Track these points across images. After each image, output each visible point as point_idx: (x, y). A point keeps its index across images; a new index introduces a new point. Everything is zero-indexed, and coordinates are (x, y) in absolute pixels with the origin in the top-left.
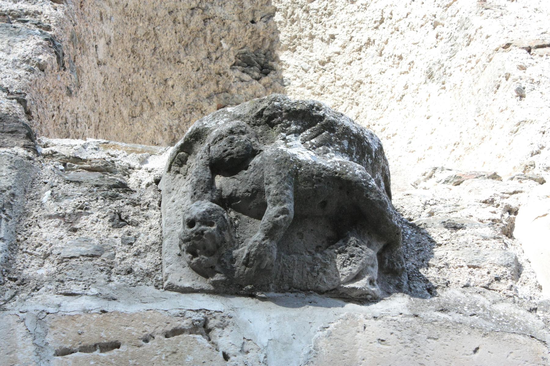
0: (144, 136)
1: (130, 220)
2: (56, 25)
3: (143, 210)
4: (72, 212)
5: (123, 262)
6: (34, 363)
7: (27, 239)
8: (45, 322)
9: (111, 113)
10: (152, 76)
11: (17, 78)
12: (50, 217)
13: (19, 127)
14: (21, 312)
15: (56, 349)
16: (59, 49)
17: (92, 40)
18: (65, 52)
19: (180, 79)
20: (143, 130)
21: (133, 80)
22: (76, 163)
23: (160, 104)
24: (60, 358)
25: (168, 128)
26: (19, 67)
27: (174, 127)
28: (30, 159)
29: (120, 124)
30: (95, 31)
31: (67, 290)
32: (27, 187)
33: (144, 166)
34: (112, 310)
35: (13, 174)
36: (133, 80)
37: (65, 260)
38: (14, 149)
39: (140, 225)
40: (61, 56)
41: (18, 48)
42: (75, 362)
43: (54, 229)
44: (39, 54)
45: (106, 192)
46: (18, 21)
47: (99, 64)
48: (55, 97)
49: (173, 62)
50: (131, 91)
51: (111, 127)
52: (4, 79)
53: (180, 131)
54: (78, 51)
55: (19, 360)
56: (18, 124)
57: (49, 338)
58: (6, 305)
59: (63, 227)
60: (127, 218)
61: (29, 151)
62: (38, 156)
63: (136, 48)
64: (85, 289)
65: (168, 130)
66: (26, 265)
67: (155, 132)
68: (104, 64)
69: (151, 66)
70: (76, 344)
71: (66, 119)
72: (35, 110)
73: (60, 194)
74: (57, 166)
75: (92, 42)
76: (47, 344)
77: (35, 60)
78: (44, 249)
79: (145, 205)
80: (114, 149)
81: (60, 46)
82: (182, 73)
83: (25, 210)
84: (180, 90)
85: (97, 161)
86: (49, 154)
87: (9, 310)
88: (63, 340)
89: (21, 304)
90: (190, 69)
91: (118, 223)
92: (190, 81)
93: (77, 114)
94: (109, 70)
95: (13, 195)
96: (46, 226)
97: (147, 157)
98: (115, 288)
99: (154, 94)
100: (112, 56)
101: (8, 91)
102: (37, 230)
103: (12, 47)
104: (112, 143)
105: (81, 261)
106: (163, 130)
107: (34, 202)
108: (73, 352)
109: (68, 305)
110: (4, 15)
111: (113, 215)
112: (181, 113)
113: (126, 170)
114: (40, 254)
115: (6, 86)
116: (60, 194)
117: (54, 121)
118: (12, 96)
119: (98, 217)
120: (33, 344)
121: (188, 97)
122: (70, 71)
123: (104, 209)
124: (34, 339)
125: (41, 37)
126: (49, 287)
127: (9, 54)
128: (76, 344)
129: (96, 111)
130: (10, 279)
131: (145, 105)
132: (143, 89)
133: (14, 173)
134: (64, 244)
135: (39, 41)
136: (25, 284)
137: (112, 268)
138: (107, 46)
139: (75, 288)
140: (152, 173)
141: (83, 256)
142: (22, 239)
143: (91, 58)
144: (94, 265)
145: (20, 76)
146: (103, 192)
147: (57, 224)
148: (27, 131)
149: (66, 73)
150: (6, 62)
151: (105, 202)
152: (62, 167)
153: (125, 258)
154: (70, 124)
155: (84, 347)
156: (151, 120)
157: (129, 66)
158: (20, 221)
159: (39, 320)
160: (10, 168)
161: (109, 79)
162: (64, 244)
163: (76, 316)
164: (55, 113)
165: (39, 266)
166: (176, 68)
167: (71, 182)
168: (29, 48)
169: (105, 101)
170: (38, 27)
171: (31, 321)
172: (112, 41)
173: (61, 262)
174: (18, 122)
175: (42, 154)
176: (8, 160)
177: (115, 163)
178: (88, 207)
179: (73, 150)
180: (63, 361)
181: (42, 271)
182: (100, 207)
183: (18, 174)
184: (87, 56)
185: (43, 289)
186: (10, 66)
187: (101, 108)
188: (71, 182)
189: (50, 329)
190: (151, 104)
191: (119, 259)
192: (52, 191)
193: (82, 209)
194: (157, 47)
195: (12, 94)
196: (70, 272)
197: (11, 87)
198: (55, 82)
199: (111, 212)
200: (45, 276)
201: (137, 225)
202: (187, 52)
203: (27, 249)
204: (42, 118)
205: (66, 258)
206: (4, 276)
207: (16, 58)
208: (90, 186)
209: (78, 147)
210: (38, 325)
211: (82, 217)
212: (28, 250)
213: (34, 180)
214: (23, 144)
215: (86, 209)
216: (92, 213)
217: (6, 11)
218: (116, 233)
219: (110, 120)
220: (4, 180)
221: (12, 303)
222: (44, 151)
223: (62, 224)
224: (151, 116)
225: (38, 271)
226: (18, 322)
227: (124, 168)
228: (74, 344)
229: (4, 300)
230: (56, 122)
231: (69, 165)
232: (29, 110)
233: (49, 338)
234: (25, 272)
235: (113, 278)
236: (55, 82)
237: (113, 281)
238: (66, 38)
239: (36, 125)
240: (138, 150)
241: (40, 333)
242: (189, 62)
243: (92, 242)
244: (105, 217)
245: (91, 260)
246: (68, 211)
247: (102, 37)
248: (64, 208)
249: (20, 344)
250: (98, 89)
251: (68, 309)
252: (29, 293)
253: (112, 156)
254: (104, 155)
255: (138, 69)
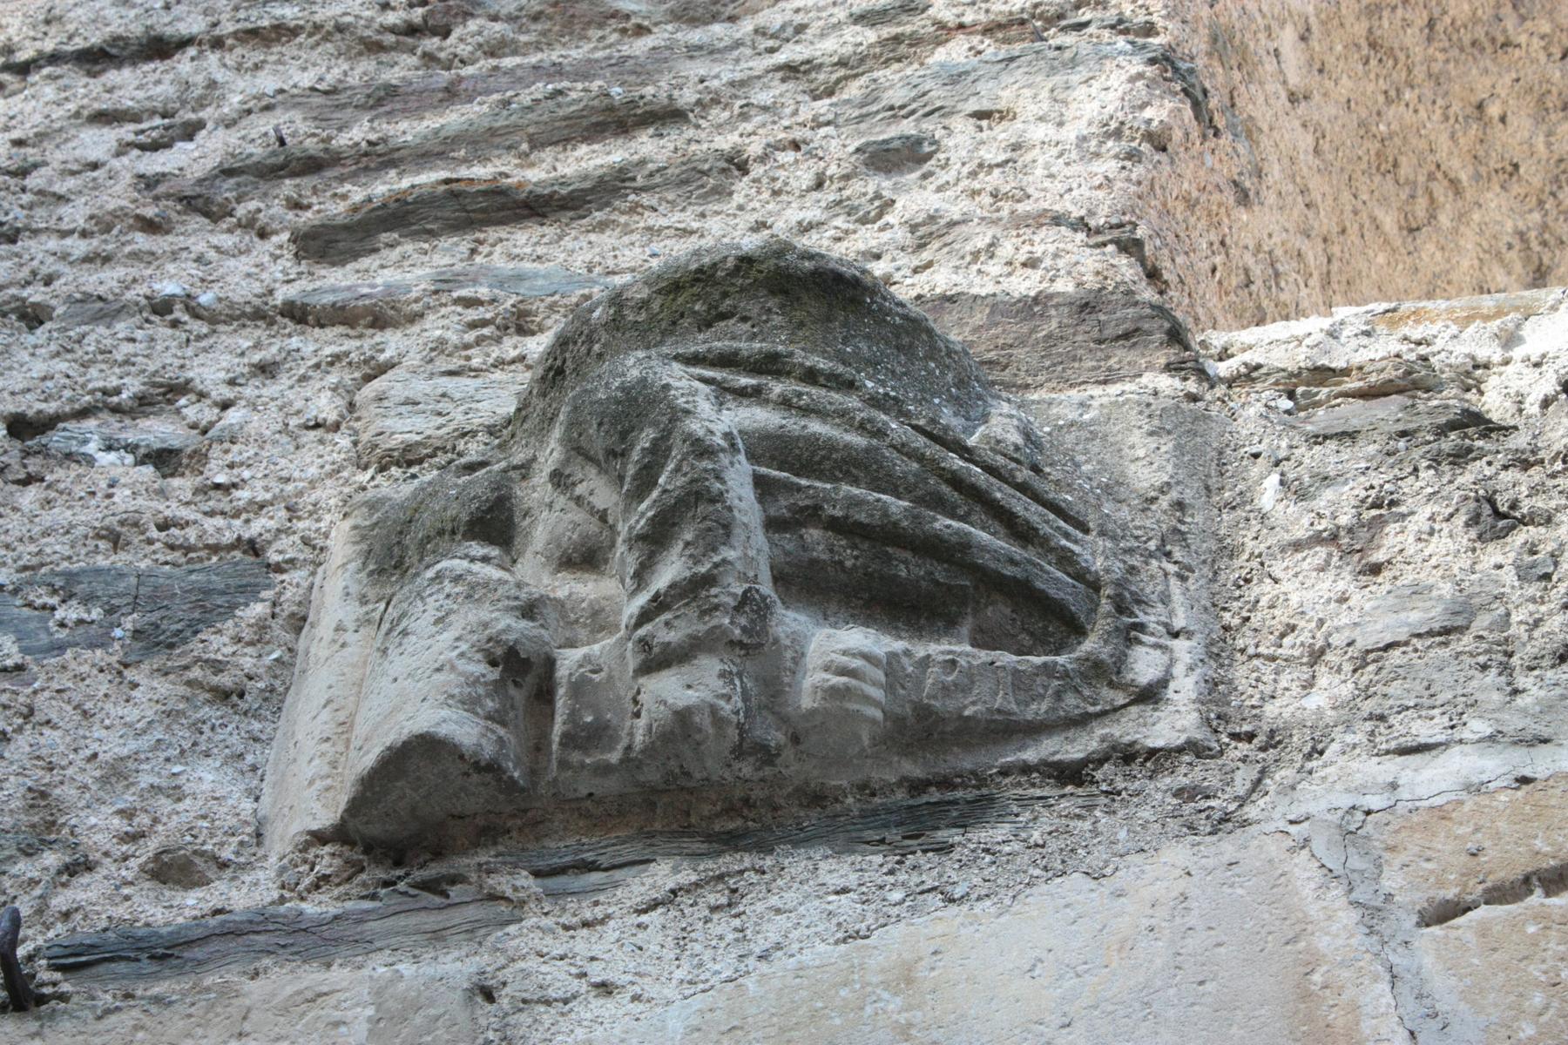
0: (1454, 276)
1: (1525, 511)
2: (1168, 17)
3: (1553, 476)
4: (1355, 521)
5: (1536, 634)
6: (1368, 956)
7: (1248, 619)
8: (1367, 838)
9: (1353, 230)
10: (1440, 102)
11: (1100, 187)
12: (1297, 546)
13: (1142, 318)
14: (1292, 822)
15: (1418, 907)
16: (1193, 80)
17: (1262, 36)
18: (1207, 85)
19: (1518, 94)
20: (1448, 261)
21: (1389, 125)
22: (1321, 384)
23: (1477, 177)
24: (1436, 930)
25: (1516, 242)
26: (1097, 155)
27: (1533, 234)
28: (1194, 398)
29: (1381, 259)
30: (1265, 8)
31: (1402, 740)
32: (1208, 476)
33: (1517, 353)
34: (1548, 773)
35: (1164, 449)
36: (1389, 125)
37: (1371, 656)
38: (1144, 380)
39: (1556, 520)
40: (1200, 97)
41: (1081, 102)
42: (1484, 936)
43: (1318, 578)
44: (1143, 106)
45: (1435, 445)
46: (1063, 29)
47: (1293, 98)
48: (1209, 215)
49: (1489, 50)
50: (1391, 159)
51: (1360, 272)
52: (1066, 196)
53: (1552, 242)
54: (1237, 75)
55: (1324, 956)
56: (1137, 309)
57: (1392, 881)
58: (1246, 809)
59: (1340, 567)
60: (1514, 505)
61: (1185, 379)
62: (1212, 387)
63: (1379, 33)
64: (1452, 727)
65: (1518, 245)
66: (1268, 690)
67: (1481, 260)
68: (1305, 98)
69: (1430, 76)
70: (1471, 883)
71: (1246, 271)
72: (1168, 264)
73: (1306, 479)
74: (1273, 404)
75: (1263, 42)
76: (1389, 897)
77: (1136, 125)
78: (1305, 637)
79: (1554, 459)
80: (1417, 322)
81: (1191, 71)
82: (1522, 74)
83: (1220, 541)
84: (1527, 123)
85: (1379, 365)
86: (1239, 376)
87: (1258, 822)
88: (1432, 880)
89: (1287, 800)
90: (1542, 57)
91: (1493, 527)
92: (1549, 92)
93: (1270, 253)
94: (1323, 111)
95: (1180, 505)
96: (1291, 573)
97: (1518, 326)
98: (1538, 708)
99: (1456, 152)
100: (1321, 71)
101: (1086, 225)
102: (1269, 588)
103: (1065, 102)
104: (1407, 306)
105: (1416, 650)
106: (1504, 250)
107: (1240, 513)
108: (1469, 909)
109: (1419, 779)
110: (1023, 22)
111: (1472, 505)
112: (1543, 191)
113: (1468, 374)
114: (1296, 653)
115: (1076, 213)
116: (1306, 479)
117: (1220, 283)
118: (1100, 239)
119: (1432, 518)
120: (1351, 903)
121: (1552, 139)
122: (1231, 137)
123: (1444, 493)
124: (1351, 891)
125: (1136, 59)
126: (1349, 738)
127: (1061, 124)
128: (1471, 883)
129: (1313, 234)
130: (1235, 736)
131: (1439, 189)
132: (1422, 145)
133: (1167, 445)
134: (1356, 612)
135: (1134, 71)
136: (1280, 742)
137: (1510, 655)
138: (1303, 45)
139: (1423, 731)
140: (1544, 368)
141: (1419, 636)
142: (1236, 621)
143: (1271, 87)
144: (1458, 654)
145: (1106, 178)
146: (1427, 448)
147: (1321, 562)
148: (1167, 325)
149: (1222, 142)
150: (1060, 147)
151: (1439, 474)
152: (1289, 404)
153: (1541, 620)
154: (1259, 283)
155: (1495, 889)
156: (1462, 229)
157: (1371, 87)
158: (1215, 573)
159: (1348, 835)
160: (1151, 434)
161: (1328, 138)
162: (1356, 612)
163: (1450, 807)
164: (1218, 260)
165: (1304, 687)
166: (1500, 65)
167: (1326, 437)
168: (1111, 95)
169: (1329, 200)
170: (1121, 32)
171: (1329, 841)
172: (1315, 28)
173: (1361, 664)
174: (1136, 303)
175: (1221, 380)
176: (1141, 413)
177: (1432, 360)
178: (1395, 497)
179: (1304, 349)
180: (1446, 936)
181: (1317, 700)
182: (1430, 490)
183: (1178, 447)
184: (1261, 83)
185: (1335, 747)
186: (1074, 155)
187: (1325, 221)
188: (1326, 437)
189: (1387, 855)
190: (1454, 183)
191: (1523, 627)
192: (1282, 474)
193: (1380, 506)
194: (1436, 15)
195: (1098, 232)
196: (1395, 688)
197: (1091, 213)
198: (1202, 173)
199: (1466, 498)
200: (1329, 713)
201: (1549, 520)
202: (1523, 11)
203: (1257, 646)
204: (1189, 280)
205: (1372, 651)
206: (1216, 731)
207: (1085, 132)
208: (1385, 437)
209: (1318, 337)
210: (1351, 850)
211: (1387, 530)
212: (1261, 650)
213: (1221, 453)
214: (1163, 361)
215: (1392, 503)
216: (1412, 513)
217: (1023, 10)
218: (1493, 555)
219: (1353, 250)
220: (1146, 471)
221: (1261, 802)
222: (1223, 369)
223: (1335, 559)
224: (1461, 216)
225: (1305, 702)
226: (1292, 850)
227: (1461, 370)
228: (1465, 885)
229: (1236, 798)
230: (1225, 284)
231: (1303, 395)
232: (1154, 266)
233: (1392, 881)
234: (1270, 710)
235: (1522, 681)
236: (1202, 173)
237: (1524, 691)
238: (1199, 44)
239: (1179, 304)
240: (1485, 311)
241: (1362, 872)
242: (1535, 40)
243: (1435, 593)
244: (1452, 515)
245: (1445, 644)
246: (1344, 520)
247: (1284, 22)
248: (1327, 513)
249: (1314, 910)
250: (1305, 170)
251: (1422, 791)
252: (1298, 765)
253: (1419, 343)
254: (1395, 347)
255: (1398, 90)
